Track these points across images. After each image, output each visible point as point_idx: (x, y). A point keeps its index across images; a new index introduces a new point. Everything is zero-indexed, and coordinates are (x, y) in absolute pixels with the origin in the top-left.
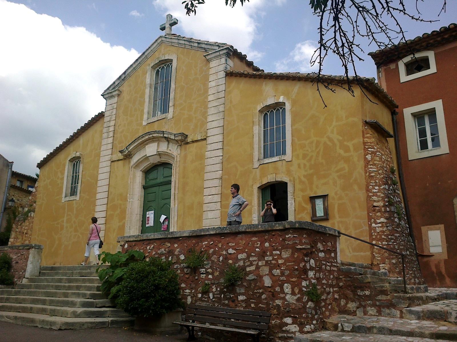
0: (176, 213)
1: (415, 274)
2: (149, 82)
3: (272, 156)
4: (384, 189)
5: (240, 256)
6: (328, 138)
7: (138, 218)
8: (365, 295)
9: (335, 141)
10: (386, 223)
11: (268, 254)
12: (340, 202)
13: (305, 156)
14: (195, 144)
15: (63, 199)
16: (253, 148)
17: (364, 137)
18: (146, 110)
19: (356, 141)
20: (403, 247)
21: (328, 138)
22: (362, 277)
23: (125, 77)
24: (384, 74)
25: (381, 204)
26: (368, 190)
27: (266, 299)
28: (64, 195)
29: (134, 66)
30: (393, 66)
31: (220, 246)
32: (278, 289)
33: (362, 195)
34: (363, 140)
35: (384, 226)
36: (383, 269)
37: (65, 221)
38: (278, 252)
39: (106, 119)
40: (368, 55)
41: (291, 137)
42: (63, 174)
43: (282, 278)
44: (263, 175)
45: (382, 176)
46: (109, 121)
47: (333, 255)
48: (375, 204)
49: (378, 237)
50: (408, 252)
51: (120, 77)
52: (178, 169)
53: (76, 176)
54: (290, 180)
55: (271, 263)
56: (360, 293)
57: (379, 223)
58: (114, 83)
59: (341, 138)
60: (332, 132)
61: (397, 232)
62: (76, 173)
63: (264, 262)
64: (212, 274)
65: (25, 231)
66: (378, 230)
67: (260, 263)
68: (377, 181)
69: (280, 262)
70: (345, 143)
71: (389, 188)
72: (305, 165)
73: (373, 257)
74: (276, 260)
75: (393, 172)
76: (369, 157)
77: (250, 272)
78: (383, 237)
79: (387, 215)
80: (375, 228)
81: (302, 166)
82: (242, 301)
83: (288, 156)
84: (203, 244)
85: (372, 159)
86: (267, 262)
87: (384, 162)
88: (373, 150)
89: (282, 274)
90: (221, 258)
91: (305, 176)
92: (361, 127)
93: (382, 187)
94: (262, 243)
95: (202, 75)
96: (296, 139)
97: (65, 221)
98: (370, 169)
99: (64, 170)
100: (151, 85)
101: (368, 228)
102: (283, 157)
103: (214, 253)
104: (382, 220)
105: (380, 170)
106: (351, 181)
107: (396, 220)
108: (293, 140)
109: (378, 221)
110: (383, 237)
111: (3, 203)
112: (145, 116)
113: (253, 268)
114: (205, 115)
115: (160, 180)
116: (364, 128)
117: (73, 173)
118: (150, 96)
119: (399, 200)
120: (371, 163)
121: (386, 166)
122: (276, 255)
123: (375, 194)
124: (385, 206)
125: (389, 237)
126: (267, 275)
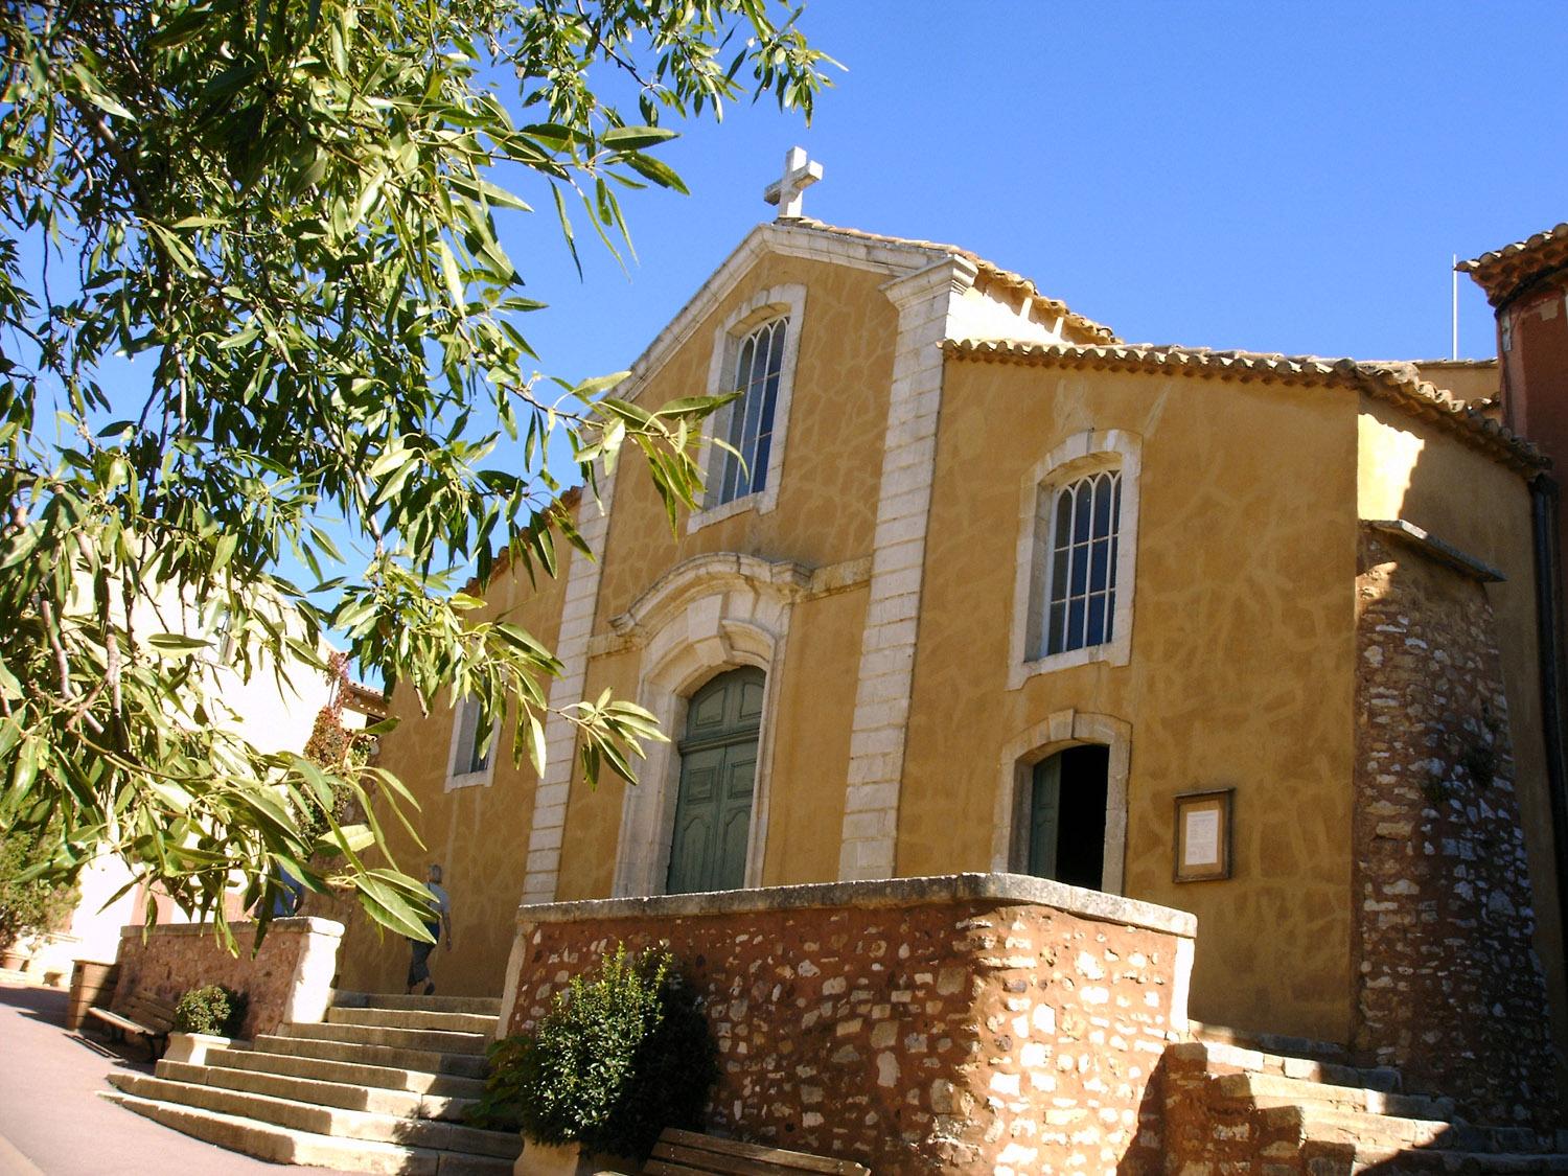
3: (1074, 644)
8: (1231, 1142)
15: (449, 779)
20: (1474, 988)
24: (1517, 337)
25: (1405, 828)
26: (1361, 775)
27: (875, 1126)
28: (450, 770)
29: (676, 330)
31: (780, 952)
33: (1336, 789)
38: (928, 978)
41: (1132, 579)
43: (928, 1063)
44: (1034, 720)
45: (1420, 727)
47: (1153, 999)
48: (1383, 829)
50: (1498, 1010)
54: (1119, 735)
55: (906, 1013)
59: (1290, 586)
61: (1457, 932)
63: (888, 1007)
64: (748, 1040)
67: (876, 1013)
68: (1398, 745)
73: (1361, 1018)
74: (922, 1003)
76: (1374, 656)
77: (848, 1039)
78: (1400, 947)
80: (1377, 913)
82: (812, 1130)
83: (1116, 651)
85: (1384, 664)
86: (895, 1006)
88: (1391, 629)
89: (933, 1041)
90: (776, 993)
92: (1354, 546)
93: (1413, 767)
97: (449, 857)
98: (1374, 701)
102: (1102, 653)
104: (1402, 887)
105: (1412, 704)
106: (1310, 743)
109: (1387, 890)
110: (1400, 947)
113: (854, 1027)
114: (872, 495)
115: (731, 721)
116: (1364, 549)
120: (1379, 678)
122: (924, 986)
123: (1384, 793)
125: (1424, 949)
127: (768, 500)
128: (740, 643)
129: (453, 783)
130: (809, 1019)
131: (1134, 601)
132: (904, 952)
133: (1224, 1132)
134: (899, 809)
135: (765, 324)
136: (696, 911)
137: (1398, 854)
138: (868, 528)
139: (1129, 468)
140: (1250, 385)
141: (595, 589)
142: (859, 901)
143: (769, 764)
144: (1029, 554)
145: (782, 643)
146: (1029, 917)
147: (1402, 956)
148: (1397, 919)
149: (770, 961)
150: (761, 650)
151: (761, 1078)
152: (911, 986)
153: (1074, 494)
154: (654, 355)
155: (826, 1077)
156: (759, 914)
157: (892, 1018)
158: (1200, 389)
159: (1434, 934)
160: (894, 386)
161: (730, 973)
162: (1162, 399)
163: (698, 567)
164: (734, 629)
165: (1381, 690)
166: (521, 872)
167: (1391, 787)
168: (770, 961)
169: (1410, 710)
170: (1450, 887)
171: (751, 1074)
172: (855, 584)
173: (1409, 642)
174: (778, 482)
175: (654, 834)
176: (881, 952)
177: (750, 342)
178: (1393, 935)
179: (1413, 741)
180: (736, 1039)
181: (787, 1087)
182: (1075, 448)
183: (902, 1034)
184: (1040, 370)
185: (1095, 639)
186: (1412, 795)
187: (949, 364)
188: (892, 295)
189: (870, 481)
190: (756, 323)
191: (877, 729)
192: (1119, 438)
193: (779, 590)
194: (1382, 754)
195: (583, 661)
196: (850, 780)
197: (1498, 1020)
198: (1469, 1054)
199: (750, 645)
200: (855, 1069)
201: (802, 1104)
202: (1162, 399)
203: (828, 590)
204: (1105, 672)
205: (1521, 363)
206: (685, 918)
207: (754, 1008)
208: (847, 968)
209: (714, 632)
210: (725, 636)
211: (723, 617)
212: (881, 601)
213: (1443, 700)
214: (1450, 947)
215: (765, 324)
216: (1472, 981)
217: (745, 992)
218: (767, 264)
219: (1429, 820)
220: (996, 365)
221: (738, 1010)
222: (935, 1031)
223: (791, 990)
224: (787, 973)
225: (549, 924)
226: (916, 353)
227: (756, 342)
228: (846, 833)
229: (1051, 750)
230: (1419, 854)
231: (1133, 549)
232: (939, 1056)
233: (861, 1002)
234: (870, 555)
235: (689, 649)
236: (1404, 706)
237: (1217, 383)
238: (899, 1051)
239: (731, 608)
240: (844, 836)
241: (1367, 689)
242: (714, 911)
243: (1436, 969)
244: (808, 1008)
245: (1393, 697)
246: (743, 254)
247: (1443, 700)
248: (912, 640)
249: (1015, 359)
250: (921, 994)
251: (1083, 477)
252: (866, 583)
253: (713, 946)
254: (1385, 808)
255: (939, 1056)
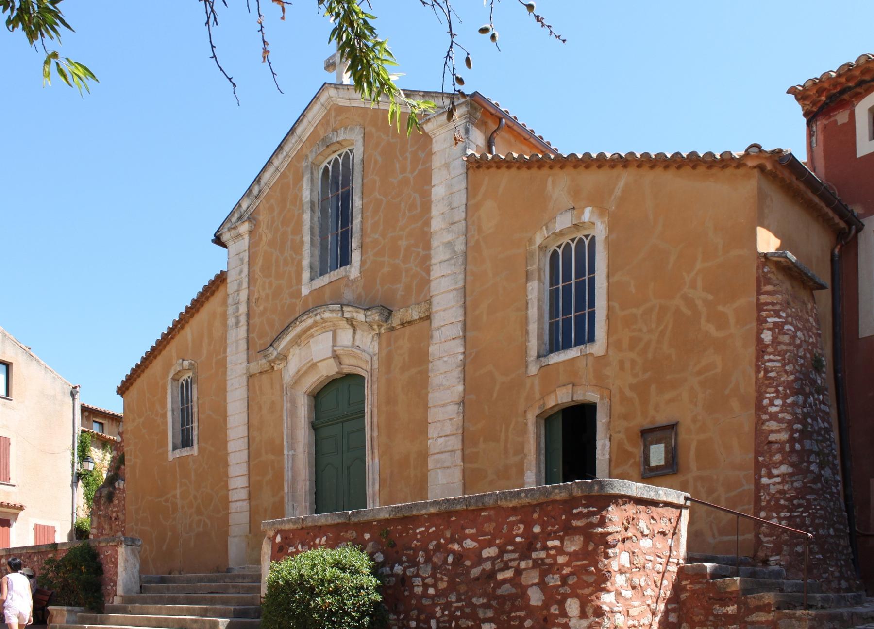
0: (377, 477)
1: (840, 572)
2: (309, 199)
3: (567, 346)
4: (795, 404)
5: (487, 553)
6: (685, 298)
7: (308, 487)
8: (726, 615)
9: (699, 303)
10: (791, 475)
11: (539, 546)
12: (702, 437)
13: (634, 343)
14: (408, 329)
15: (170, 453)
16: (527, 333)
17: (759, 292)
18: (306, 262)
19: (742, 302)
20: (821, 521)
21: (685, 298)
22: (724, 582)
23: (260, 191)
24: (821, 137)
25: (784, 436)
26: (760, 408)
28: (170, 447)
30: (841, 117)
32: (554, 610)
33: (745, 419)
34: (758, 299)
35: (787, 483)
36: (777, 564)
37: (178, 496)
38: (557, 543)
39: (231, 285)
40: (788, 92)
42: (164, 406)
43: (562, 590)
45: (792, 377)
46: (237, 290)
48: (772, 437)
49: (772, 503)
50: (831, 531)
51: (250, 190)
52: (375, 386)
53: (187, 408)
54: (602, 398)
55: (543, 563)
56: (718, 610)
57: (778, 476)
58: (239, 205)
59: (710, 297)
60: (693, 286)
61: (812, 491)
62: (188, 403)
63: (530, 562)
64: (434, 586)
65: (114, 515)
66: (773, 490)
68: (781, 389)
69: (561, 560)
70: (720, 308)
71: (805, 401)
72: (633, 362)
73: (759, 542)
74: (554, 557)
75: (817, 365)
76: (767, 336)
77: (505, 581)
78: (782, 502)
79: (794, 458)
80: (768, 485)
81: (628, 365)
83: (598, 347)
84: (418, 531)
87: (799, 347)
88: (777, 320)
89: (564, 579)
90: (450, 559)
91: (632, 387)
93: (789, 401)
94: (529, 526)
95: (416, 172)
96: (616, 305)
98: (767, 364)
99: (165, 398)
100: (312, 203)
101: (752, 487)
103: (438, 547)
104: (784, 469)
105: (788, 364)
106: (727, 392)
107: (813, 467)
108: (609, 308)
109: (775, 472)
110: (782, 502)
111: (73, 453)
112: (306, 275)
113: (509, 574)
116: (760, 271)
117: (182, 404)
118: (312, 229)
119: (826, 425)
120: (770, 350)
121: (805, 354)
122: (554, 547)
123: (773, 417)
124: (792, 440)
125: (795, 502)
126: (535, 584)
127: (354, 270)
128: (346, 360)
129: (172, 455)
130: (475, 572)
131: (608, 316)
132: (537, 529)
133: (718, 610)
134: (463, 450)
135: (336, 155)
136: (387, 516)
137: (781, 450)
138: (425, 282)
139: (600, 232)
140: (682, 171)
141: (245, 335)
142: (503, 503)
143: (376, 429)
144: (536, 292)
145: (375, 358)
146: (617, 504)
147: (783, 507)
148: (780, 487)
149: (442, 541)
150: (361, 364)
151: (447, 606)
152: (545, 548)
153: (560, 252)
154: (264, 180)
155: (494, 603)
156: (431, 515)
157: (534, 567)
158: (649, 177)
159: (801, 493)
160: (433, 190)
161: (416, 550)
162: (621, 184)
163: (316, 315)
164: (342, 352)
165: (771, 357)
166: (226, 502)
167: (777, 413)
168: (442, 541)
169: (787, 368)
170: (808, 467)
171: (440, 605)
172: (421, 319)
173: (786, 327)
174: (359, 259)
175: (305, 476)
176: (521, 530)
177: (326, 169)
178: (778, 496)
179: (788, 385)
180: (426, 586)
181: (468, 610)
182: (563, 222)
183: (543, 575)
184: (534, 171)
185: (580, 341)
186: (788, 417)
187: (470, 172)
188: (428, 128)
189: (422, 253)
190: (329, 155)
191: (444, 405)
192: (592, 212)
193: (371, 326)
194: (772, 395)
195: (244, 378)
196: (430, 436)
197: (832, 537)
198: (820, 556)
199: (353, 361)
200: (512, 597)
201: (480, 619)
202: (621, 184)
203: (402, 324)
204: (590, 358)
205: (822, 154)
206: (379, 521)
207: (435, 568)
208: (497, 541)
209: (330, 354)
210: (336, 357)
211: (333, 346)
212: (439, 329)
213: (802, 361)
214: (809, 500)
215: (336, 155)
216: (821, 517)
217: (428, 560)
218: (333, 113)
219: (797, 431)
220: (504, 170)
221: (426, 571)
222: (564, 572)
223: (459, 558)
224: (456, 547)
225: (285, 530)
226: (447, 166)
227: (330, 168)
228: (430, 467)
229: (556, 409)
230: (793, 450)
231: (605, 284)
232: (570, 586)
233: (511, 560)
234: (429, 302)
235: (314, 366)
236: (784, 366)
237: (659, 170)
238: (542, 585)
239: (339, 339)
240: (430, 468)
241: (763, 357)
242: (399, 515)
243: (802, 512)
244: (474, 566)
245: (778, 361)
246: (316, 108)
247: (802, 361)
248: (462, 350)
249: (517, 165)
250: (552, 552)
251: (565, 240)
252: (428, 318)
253: (401, 536)
254: (773, 425)
255: (570, 586)
